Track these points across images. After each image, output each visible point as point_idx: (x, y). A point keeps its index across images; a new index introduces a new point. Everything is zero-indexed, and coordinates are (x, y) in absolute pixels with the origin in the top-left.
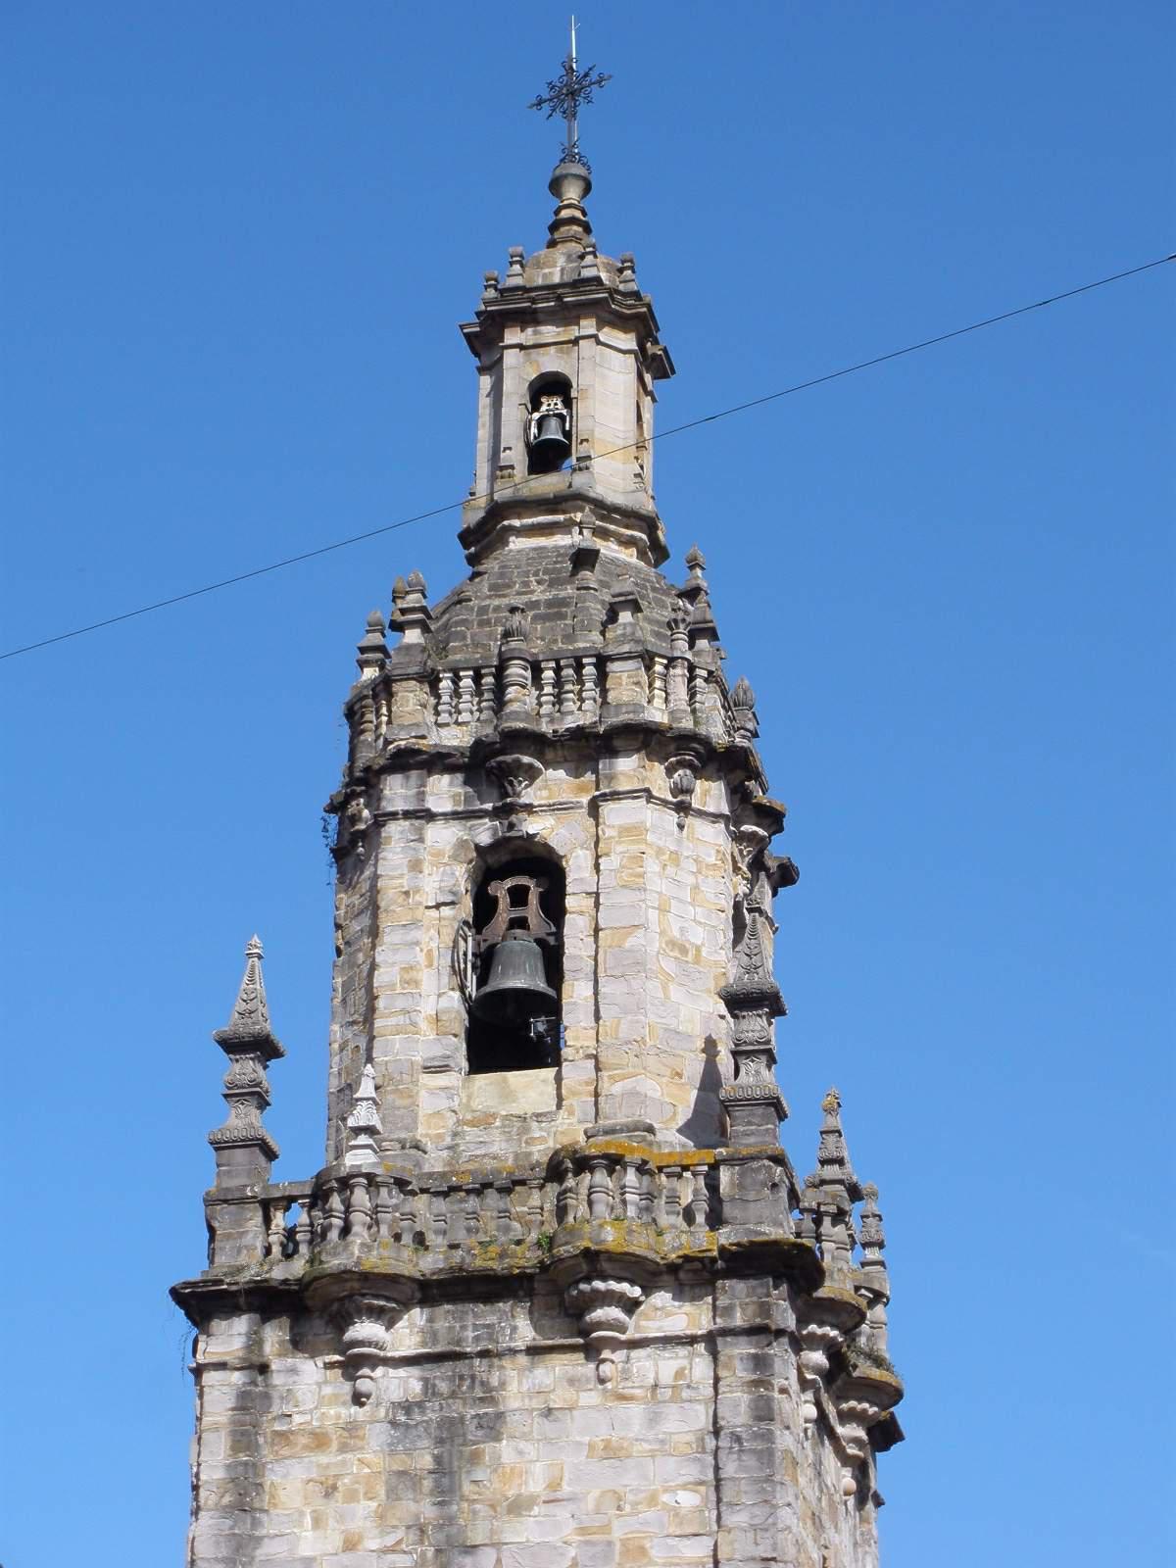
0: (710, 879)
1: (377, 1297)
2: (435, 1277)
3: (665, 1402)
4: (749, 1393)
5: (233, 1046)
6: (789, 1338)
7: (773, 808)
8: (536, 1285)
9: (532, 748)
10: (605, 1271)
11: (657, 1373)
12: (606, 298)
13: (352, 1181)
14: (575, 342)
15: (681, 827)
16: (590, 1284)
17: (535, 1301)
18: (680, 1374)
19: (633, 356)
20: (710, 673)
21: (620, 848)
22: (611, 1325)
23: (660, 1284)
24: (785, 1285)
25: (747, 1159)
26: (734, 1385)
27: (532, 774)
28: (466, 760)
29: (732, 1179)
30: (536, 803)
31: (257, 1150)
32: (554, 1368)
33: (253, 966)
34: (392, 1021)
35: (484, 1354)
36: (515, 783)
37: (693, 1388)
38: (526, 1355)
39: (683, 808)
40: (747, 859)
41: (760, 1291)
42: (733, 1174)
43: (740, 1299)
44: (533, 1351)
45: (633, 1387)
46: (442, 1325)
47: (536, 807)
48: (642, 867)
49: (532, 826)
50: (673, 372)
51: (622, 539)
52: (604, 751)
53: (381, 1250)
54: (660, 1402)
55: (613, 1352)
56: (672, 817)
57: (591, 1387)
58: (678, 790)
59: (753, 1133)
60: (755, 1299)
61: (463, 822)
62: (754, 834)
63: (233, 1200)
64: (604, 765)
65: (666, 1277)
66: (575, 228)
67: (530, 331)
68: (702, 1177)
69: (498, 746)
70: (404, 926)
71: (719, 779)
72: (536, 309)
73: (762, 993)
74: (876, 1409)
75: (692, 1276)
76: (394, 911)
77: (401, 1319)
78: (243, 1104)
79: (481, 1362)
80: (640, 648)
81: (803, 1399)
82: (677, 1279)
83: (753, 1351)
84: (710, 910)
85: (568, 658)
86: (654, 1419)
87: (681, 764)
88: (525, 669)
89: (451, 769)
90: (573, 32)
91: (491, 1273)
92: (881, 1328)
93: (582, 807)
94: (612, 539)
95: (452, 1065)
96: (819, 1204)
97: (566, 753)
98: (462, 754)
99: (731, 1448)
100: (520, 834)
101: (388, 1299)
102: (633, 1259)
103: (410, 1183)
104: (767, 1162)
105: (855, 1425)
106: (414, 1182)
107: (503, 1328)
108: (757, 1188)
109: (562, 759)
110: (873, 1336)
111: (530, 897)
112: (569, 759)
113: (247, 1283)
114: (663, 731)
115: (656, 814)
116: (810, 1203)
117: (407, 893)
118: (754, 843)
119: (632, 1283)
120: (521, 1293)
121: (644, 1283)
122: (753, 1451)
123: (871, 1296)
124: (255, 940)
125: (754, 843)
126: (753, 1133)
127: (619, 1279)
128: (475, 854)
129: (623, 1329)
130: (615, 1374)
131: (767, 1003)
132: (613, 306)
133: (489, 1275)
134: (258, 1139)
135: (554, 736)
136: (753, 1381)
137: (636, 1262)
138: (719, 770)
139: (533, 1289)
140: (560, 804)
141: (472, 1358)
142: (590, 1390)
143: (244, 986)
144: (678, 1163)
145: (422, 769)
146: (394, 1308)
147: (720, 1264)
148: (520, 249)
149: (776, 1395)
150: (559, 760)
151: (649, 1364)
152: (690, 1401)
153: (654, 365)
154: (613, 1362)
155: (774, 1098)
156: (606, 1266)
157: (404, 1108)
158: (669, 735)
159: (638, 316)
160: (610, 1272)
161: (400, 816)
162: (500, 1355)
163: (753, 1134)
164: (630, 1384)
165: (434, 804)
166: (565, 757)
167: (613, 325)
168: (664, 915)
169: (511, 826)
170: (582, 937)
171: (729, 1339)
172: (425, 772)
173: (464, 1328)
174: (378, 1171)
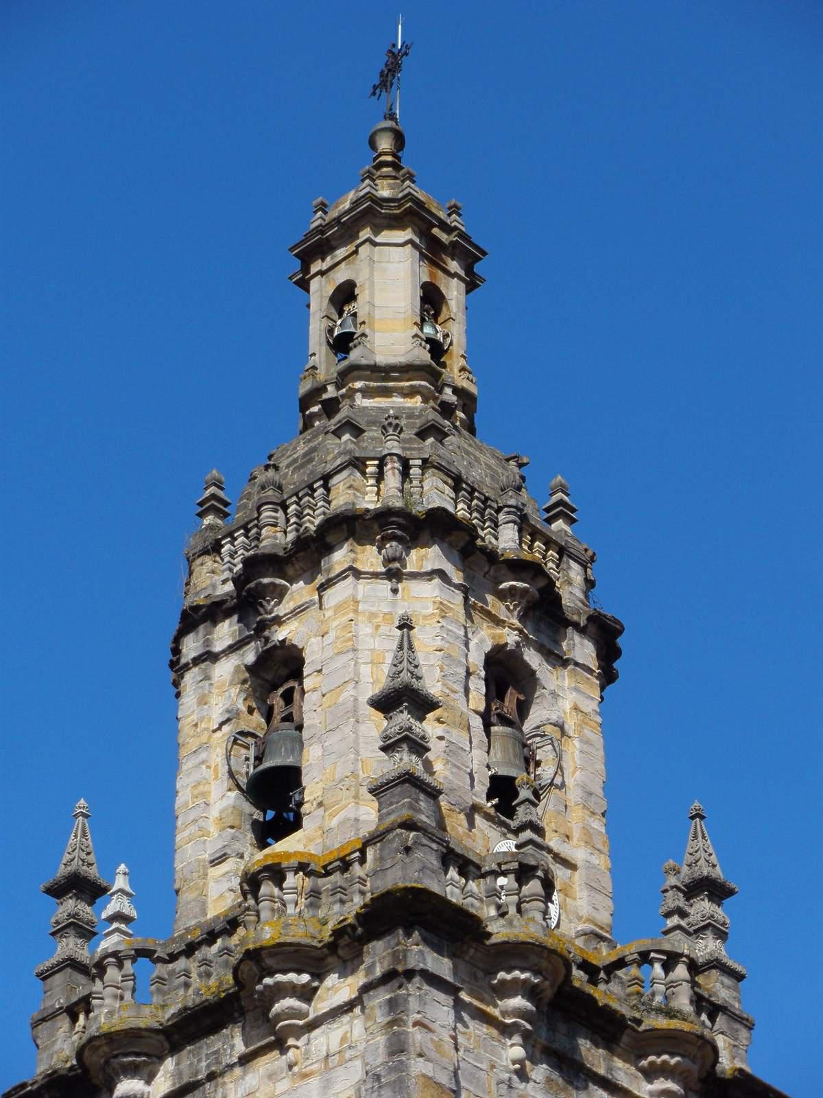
0: (428, 628)
1: (127, 1055)
2: (170, 1023)
3: (335, 1067)
4: (385, 1034)
5: (57, 891)
6: (420, 975)
7: (522, 560)
8: (243, 1004)
9: (271, 569)
10: (271, 967)
11: (328, 1045)
12: (369, 207)
13: (106, 961)
14: (356, 252)
15: (395, 591)
16: (261, 984)
17: (247, 1018)
18: (343, 1039)
19: (410, 245)
20: (425, 461)
21: (335, 624)
22: (287, 1014)
23: (327, 969)
24: (417, 932)
25: (384, 833)
26: (375, 1031)
27: (280, 593)
28: (235, 600)
29: (375, 855)
30: (281, 614)
31: (69, 970)
32: (258, 1070)
33: (84, 825)
34: (186, 833)
35: (212, 1077)
36: (265, 603)
37: (353, 1047)
38: (240, 1066)
39: (394, 574)
40: (516, 613)
41: (393, 942)
42: (376, 851)
43: (378, 956)
44: (245, 1060)
45: (312, 1064)
46: (186, 1063)
47: (283, 617)
48: (350, 632)
49: (280, 634)
50: (484, 253)
51: (405, 392)
52: (323, 550)
53: (121, 1012)
54: (332, 1069)
55: (298, 1039)
56: (385, 586)
57: (284, 1075)
58: (388, 560)
59: (393, 811)
60: (390, 951)
61: (238, 652)
62: (513, 587)
63: (48, 1016)
64: (325, 561)
65: (330, 960)
66: (385, 169)
67: (329, 258)
68: (357, 863)
69: (242, 577)
70: (195, 752)
71: (434, 543)
72: (326, 238)
73: (396, 690)
74: (678, 1059)
75: (342, 949)
76: (188, 743)
77: (158, 1071)
78: (65, 937)
79: (210, 1085)
80: (347, 457)
81: (509, 1044)
82: (339, 957)
83: (388, 997)
84: (428, 653)
85: (303, 489)
86: (327, 1085)
87: (385, 539)
88: (276, 511)
89: (228, 614)
90: (400, 26)
91: (207, 1003)
92: (681, 984)
93: (314, 604)
94: (395, 394)
95: (229, 852)
96: (499, 865)
97: (301, 564)
98: (231, 596)
99: (373, 1087)
100: (273, 643)
101: (138, 1054)
102: (292, 949)
103: (155, 951)
104: (399, 831)
105: (662, 1079)
106: (159, 949)
107: (224, 1050)
108: (392, 855)
109: (301, 572)
110: (673, 994)
111: (295, 695)
112: (305, 568)
113: (43, 1078)
114: (361, 515)
115: (368, 587)
116: (490, 866)
117: (196, 725)
118: (518, 597)
119: (299, 972)
120: (236, 1015)
121: (313, 970)
122: (388, 1084)
123: (665, 958)
124: (82, 802)
125: (518, 597)
126: (393, 811)
127: (285, 972)
128: (247, 675)
129: (301, 1015)
130: (300, 1057)
131: (404, 698)
132: (383, 211)
133: (205, 1007)
134: (67, 960)
135: (285, 553)
136: (388, 1023)
137: (296, 951)
138: (432, 537)
139: (242, 1008)
140: (299, 608)
141: (204, 1083)
142: (284, 1078)
143: (71, 841)
144: (336, 858)
145: (205, 621)
146: (145, 1061)
147: (360, 930)
148: (320, 199)
149: (411, 1030)
150: (299, 573)
151: (322, 1040)
152: (351, 1060)
153: (472, 284)
154: (297, 1048)
155: (405, 774)
156: (269, 962)
157: (193, 900)
158: (368, 517)
159: (409, 212)
160: (276, 966)
161: (191, 665)
162: (222, 1074)
163: (394, 811)
164: (311, 1061)
165: (218, 647)
166: (302, 568)
167: (391, 227)
168: (377, 668)
169: (267, 640)
170: (315, 708)
171: (371, 993)
172: (208, 623)
173: (199, 1061)
174: (120, 948)
